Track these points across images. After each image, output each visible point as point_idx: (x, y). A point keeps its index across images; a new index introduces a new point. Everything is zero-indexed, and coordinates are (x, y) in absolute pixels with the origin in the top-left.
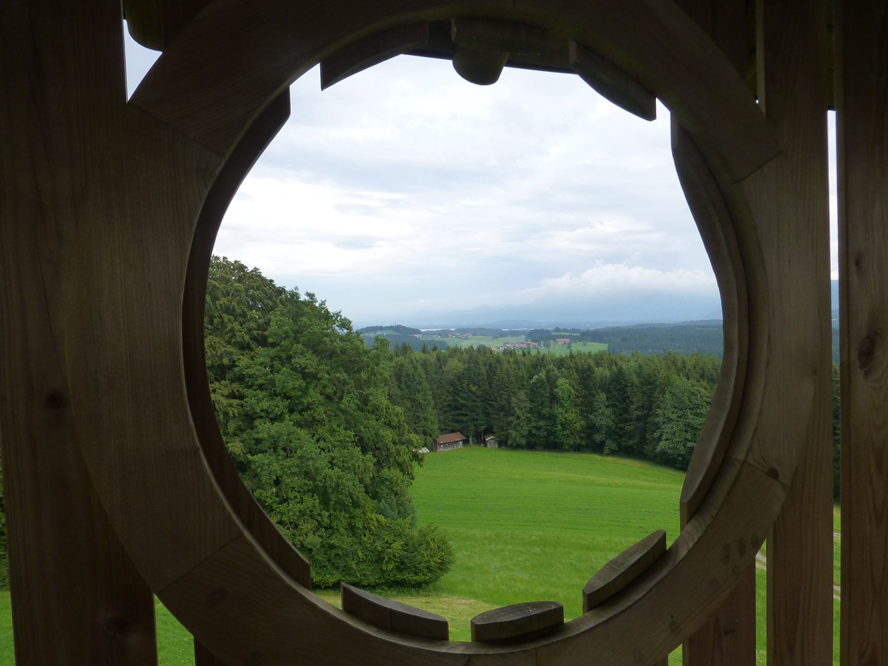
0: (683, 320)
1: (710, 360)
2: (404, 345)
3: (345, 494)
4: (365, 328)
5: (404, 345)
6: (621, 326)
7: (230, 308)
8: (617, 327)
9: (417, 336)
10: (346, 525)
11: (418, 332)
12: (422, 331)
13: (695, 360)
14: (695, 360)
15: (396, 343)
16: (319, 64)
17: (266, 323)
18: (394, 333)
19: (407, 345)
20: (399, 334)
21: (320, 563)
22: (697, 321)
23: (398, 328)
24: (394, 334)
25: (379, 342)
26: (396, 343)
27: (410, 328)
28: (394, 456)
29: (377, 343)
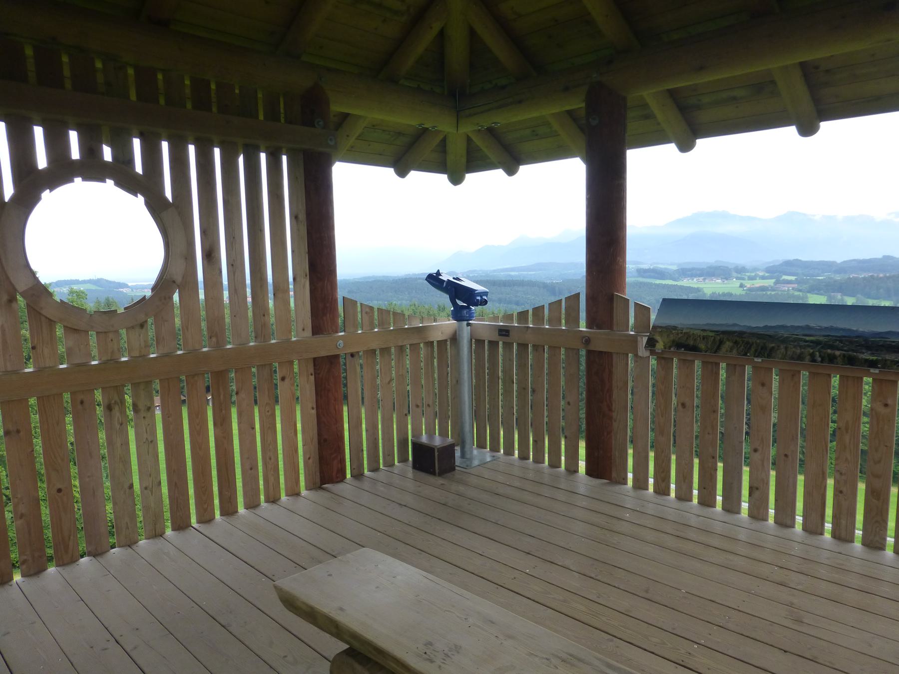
0: (407, 273)
1: (426, 309)
2: (107, 299)
3: (40, 463)
4: (55, 281)
5: (107, 299)
6: (348, 278)
7: (471, 320)
8: (365, 278)
9: (124, 290)
10: (43, 496)
11: (125, 286)
12: (130, 284)
13: (413, 310)
14: (413, 310)
15: (97, 298)
16: (104, 145)
17: (389, 304)
18: (93, 287)
19: (111, 300)
20: (100, 288)
21: (12, 540)
22: (419, 274)
23: (98, 282)
24: (94, 288)
25: (75, 295)
26: (97, 298)
27: (114, 282)
28: (99, 419)
29: (72, 296)
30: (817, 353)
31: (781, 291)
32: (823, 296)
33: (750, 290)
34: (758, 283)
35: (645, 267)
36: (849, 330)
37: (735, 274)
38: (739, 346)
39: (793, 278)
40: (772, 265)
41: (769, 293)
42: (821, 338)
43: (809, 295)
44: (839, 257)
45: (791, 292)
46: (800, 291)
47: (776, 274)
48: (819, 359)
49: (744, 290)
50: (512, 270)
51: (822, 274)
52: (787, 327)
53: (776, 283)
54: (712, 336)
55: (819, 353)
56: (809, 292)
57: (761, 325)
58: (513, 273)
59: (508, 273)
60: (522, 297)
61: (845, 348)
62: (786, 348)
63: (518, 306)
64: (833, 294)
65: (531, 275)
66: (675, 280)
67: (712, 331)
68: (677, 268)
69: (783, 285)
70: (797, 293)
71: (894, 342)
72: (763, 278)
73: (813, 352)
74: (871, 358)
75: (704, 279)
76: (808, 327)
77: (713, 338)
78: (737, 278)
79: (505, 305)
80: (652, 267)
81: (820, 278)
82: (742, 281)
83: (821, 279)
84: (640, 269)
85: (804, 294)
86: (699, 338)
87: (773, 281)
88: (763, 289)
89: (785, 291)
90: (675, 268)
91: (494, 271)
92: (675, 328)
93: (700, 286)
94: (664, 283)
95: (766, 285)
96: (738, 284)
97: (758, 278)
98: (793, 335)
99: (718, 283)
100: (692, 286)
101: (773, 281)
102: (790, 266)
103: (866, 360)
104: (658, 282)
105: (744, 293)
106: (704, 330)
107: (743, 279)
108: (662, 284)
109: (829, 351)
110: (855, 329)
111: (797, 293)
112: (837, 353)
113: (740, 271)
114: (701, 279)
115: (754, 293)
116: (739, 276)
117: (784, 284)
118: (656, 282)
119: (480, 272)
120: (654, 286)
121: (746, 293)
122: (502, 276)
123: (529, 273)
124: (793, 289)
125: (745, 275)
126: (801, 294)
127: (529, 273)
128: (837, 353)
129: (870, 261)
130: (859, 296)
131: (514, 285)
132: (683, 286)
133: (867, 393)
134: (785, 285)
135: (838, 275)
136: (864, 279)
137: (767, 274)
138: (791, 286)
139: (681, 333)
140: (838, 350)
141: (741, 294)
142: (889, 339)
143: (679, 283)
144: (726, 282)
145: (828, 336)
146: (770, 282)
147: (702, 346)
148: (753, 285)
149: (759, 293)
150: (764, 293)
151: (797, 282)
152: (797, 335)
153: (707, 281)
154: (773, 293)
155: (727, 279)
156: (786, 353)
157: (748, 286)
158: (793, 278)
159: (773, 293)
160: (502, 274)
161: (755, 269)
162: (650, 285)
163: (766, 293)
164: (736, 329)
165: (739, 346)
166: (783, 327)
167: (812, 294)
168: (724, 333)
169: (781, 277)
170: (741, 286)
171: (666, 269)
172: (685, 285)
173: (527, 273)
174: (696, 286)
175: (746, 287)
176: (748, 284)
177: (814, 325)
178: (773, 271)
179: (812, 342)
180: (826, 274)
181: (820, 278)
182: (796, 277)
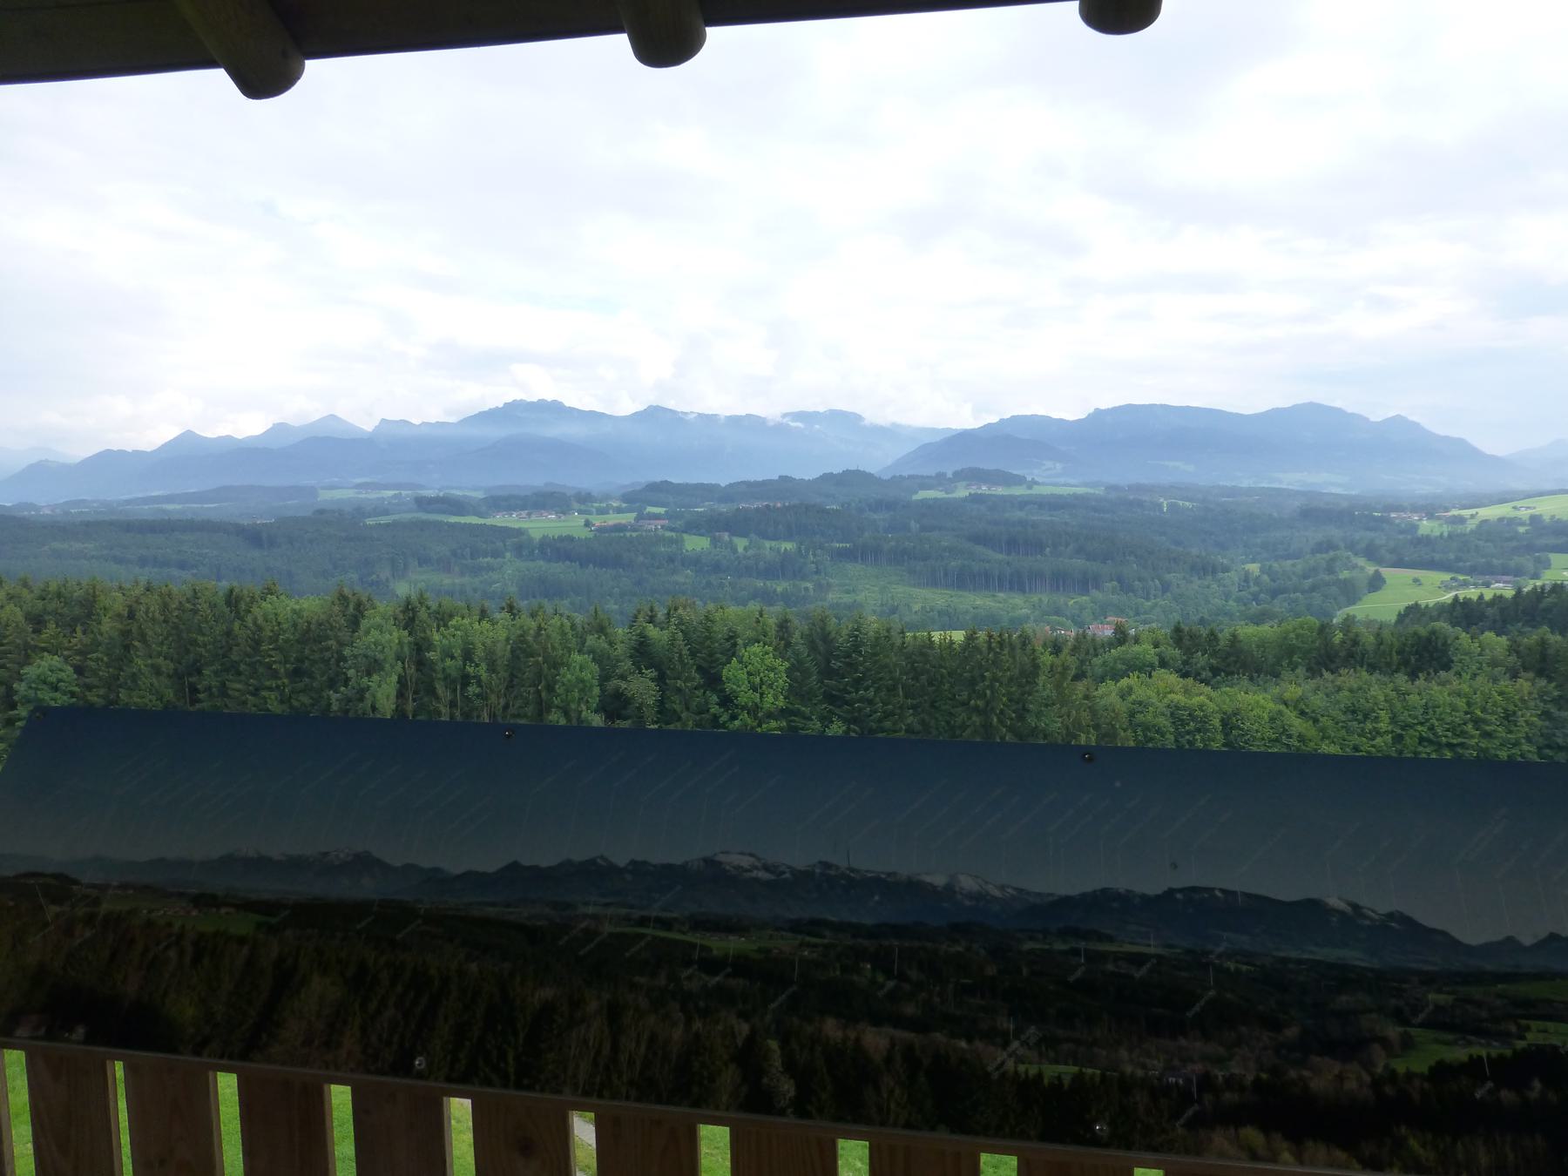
30: (773, 1044)
31: (646, 531)
32: (704, 538)
33: (601, 530)
34: (612, 519)
35: (430, 493)
36: (914, 887)
37: (576, 506)
38: (373, 1006)
39: (661, 510)
40: (631, 490)
41: (628, 534)
42: (785, 944)
43: (685, 536)
44: (723, 478)
45: (661, 532)
46: (672, 530)
47: (638, 504)
48: (788, 1087)
49: (591, 531)
50: (169, 499)
51: (701, 505)
52: (612, 870)
53: (637, 519)
54: (242, 941)
55: (785, 1042)
56: (683, 532)
57: (490, 864)
58: (170, 507)
59: (160, 506)
60: (192, 552)
61: (910, 1010)
62: (613, 1012)
63: (183, 570)
64: (717, 534)
65: (211, 510)
66: (480, 515)
67: (248, 906)
68: (484, 496)
69: (648, 521)
70: (668, 534)
71: (1138, 959)
72: (619, 511)
73: (751, 1039)
74: (1051, 1071)
75: (529, 515)
76: (714, 874)
77: (245, 950)
78: (580, 512)
79: (156, 570)
80: (441, 494)
81: (700, 510)
82: (588, 516)
83: (701, 512)
84: (422, 497)
85: (678, 534)
86: (172, 953)
87: (634, 515)
88: (619, 528)
89: (650, 531)
90: (480, 495)
91: (128, 502)
92: (60, 886)
93: (524, 525)
94: (463, 522)
95: (624, 522)
96: (582, 522)
97: (611, 512)
98: (643, 922)
99: (552, 520)
100: (509, 525)
101: (634, 515)
102: (659, 490)
103: (1028, 1089)
104: (453, 519)
105: (591, 535)
106: (205, 901)
107: (589, 513)
108: (460, 523)
109: (831, 1028)
110: (939, 880)
111: (668, 534)
112: (876, 1040)
113: (585, 499)
114: (524, 513)
115: (607, 535)
116: (583, 507)
117: (650, 519)
118: (450, 521)
119: (95, 505)
120: (446, 527)
121: (595, 535)
122: (146, 512)
123: (206, 506)
124: (662, 527)
125: (592, 506)
126: (674, 534)
127: (206, 506)
128: (876, 1040)
129: (764, 483)
130: (752, 535)
131: (173, 531)
132: (495, 526)
133: (773, 684)
134: (652, 522)
135: (723, 505)
136: (757, 509)
137: (624, 505)
138: (659, 523)
139: (90, 920)
140: (877, 1020)
141: (588, 537)
142: (1110, 939)
143: (489, 521)
144: (563, 518)
145: (814, 926)
146: (628, 518)
147: (184, 1010)
148: (605, 522)
149: (613, 534)
150: (622, 534)
151: (668, 516)
152: (666, 924)
153: (533, 517)
154: (634, 534)
155: (564, 514)
156: (615, 1048)
157: (597, 523)
158: (661, 510)
159: (634, 534)
160: (146, 507)
161: (607, 497)
162: (438, 525)
163: (625, 535)
164: (367, 888)
165: (373, 1006)
166: (595, 873)
167: (690, 534)
168: (312, 914)
169: (645, 509)
170: (587, 524)
171: (465, 496)
172: (499, 525)
173: (199, 506)
174: (516, 526)
175: (594, 525)
176: (598, 521)
177: (745, 862)
178: (635, 499)
179: (741, 966)
180: (707, 503)
181: (700, 510)
182: (665, 509)
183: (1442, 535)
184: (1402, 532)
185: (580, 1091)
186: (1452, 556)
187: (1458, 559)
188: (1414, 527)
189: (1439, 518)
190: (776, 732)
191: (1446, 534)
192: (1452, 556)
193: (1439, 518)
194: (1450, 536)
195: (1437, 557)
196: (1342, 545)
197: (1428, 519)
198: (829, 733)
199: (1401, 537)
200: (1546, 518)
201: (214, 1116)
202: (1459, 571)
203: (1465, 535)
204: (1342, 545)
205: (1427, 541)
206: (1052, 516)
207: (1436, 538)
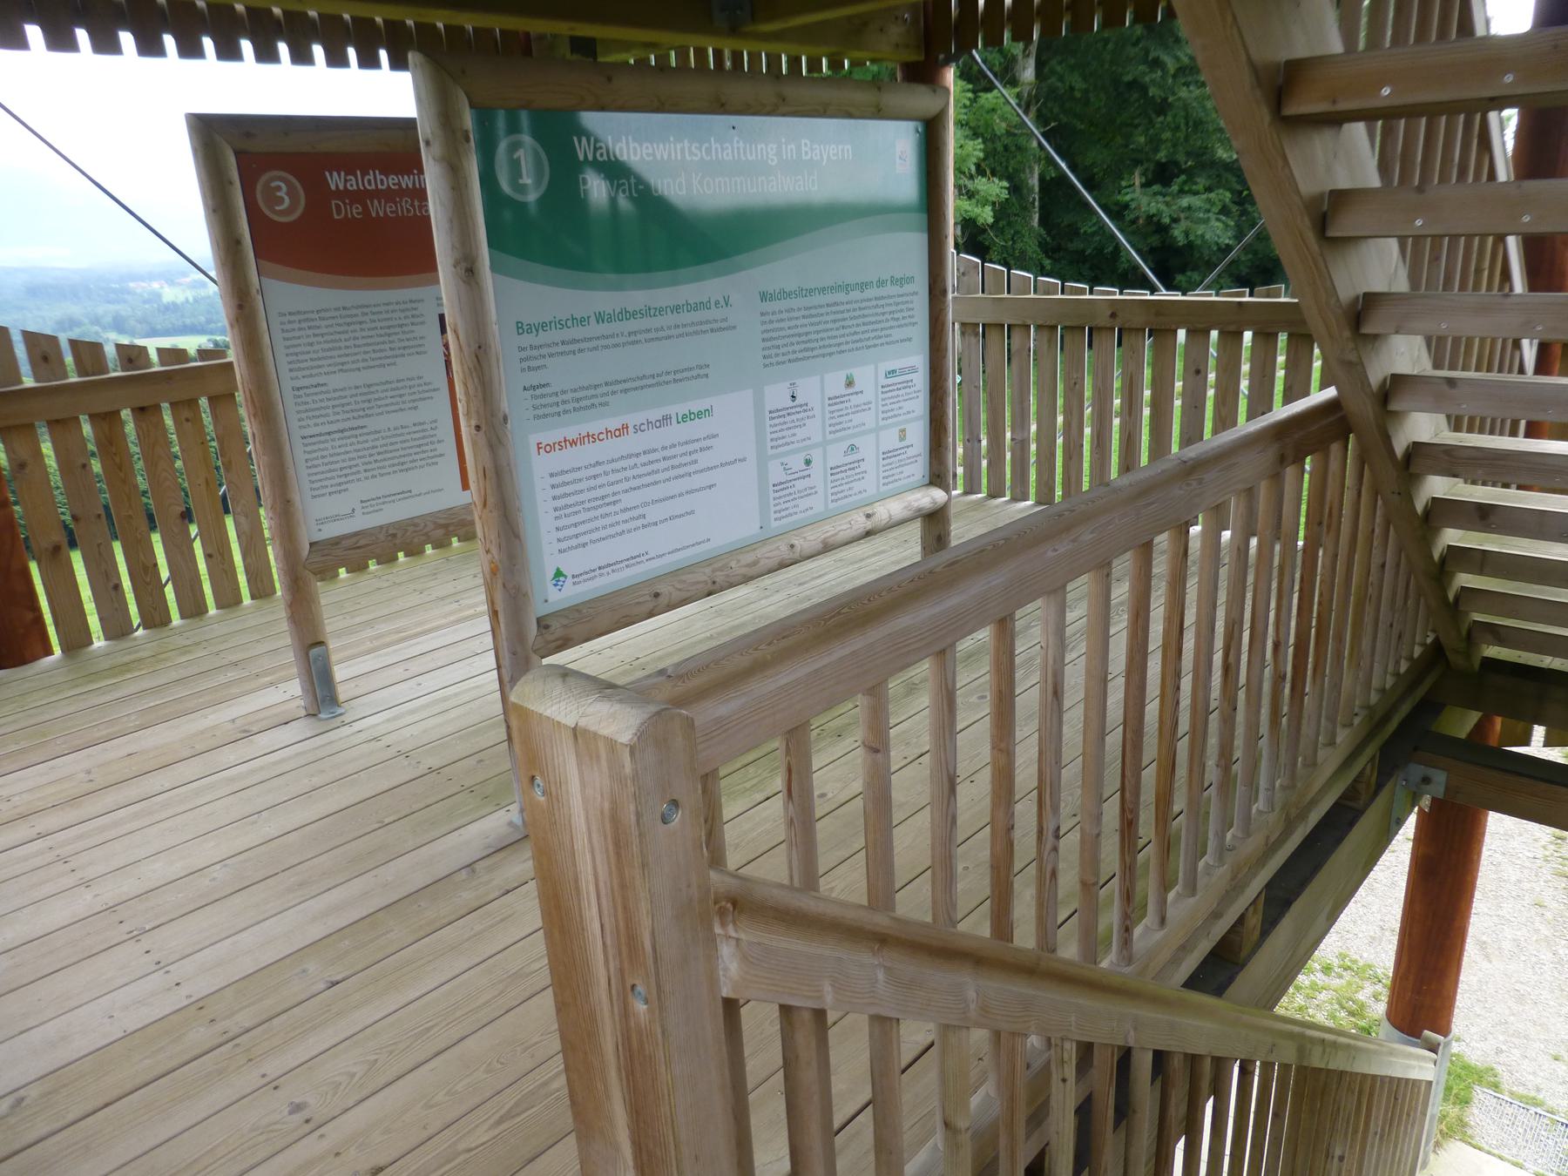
183: (187, 301)
184: (145, 302)
185: (407, 182)
186: (202, 319)
187: (209, 321)
188: (159, 296)
189: (180, 284)
190: (1306, 485)
191: (191, 299)
192: (202, 319)
193: (180, 284)
194: (196, 300)
195: (188, 321)
196: (86, 321)
197: (170, 285)
198: (1474, 717)
199: (147, 306)
200: (602, 175)
201: (1108, 443)
202: (211, 333)
203: (209, 297)
204: (86, 321)
205: (173, 308)
206: (1285, 765)
207: (182, 304)
